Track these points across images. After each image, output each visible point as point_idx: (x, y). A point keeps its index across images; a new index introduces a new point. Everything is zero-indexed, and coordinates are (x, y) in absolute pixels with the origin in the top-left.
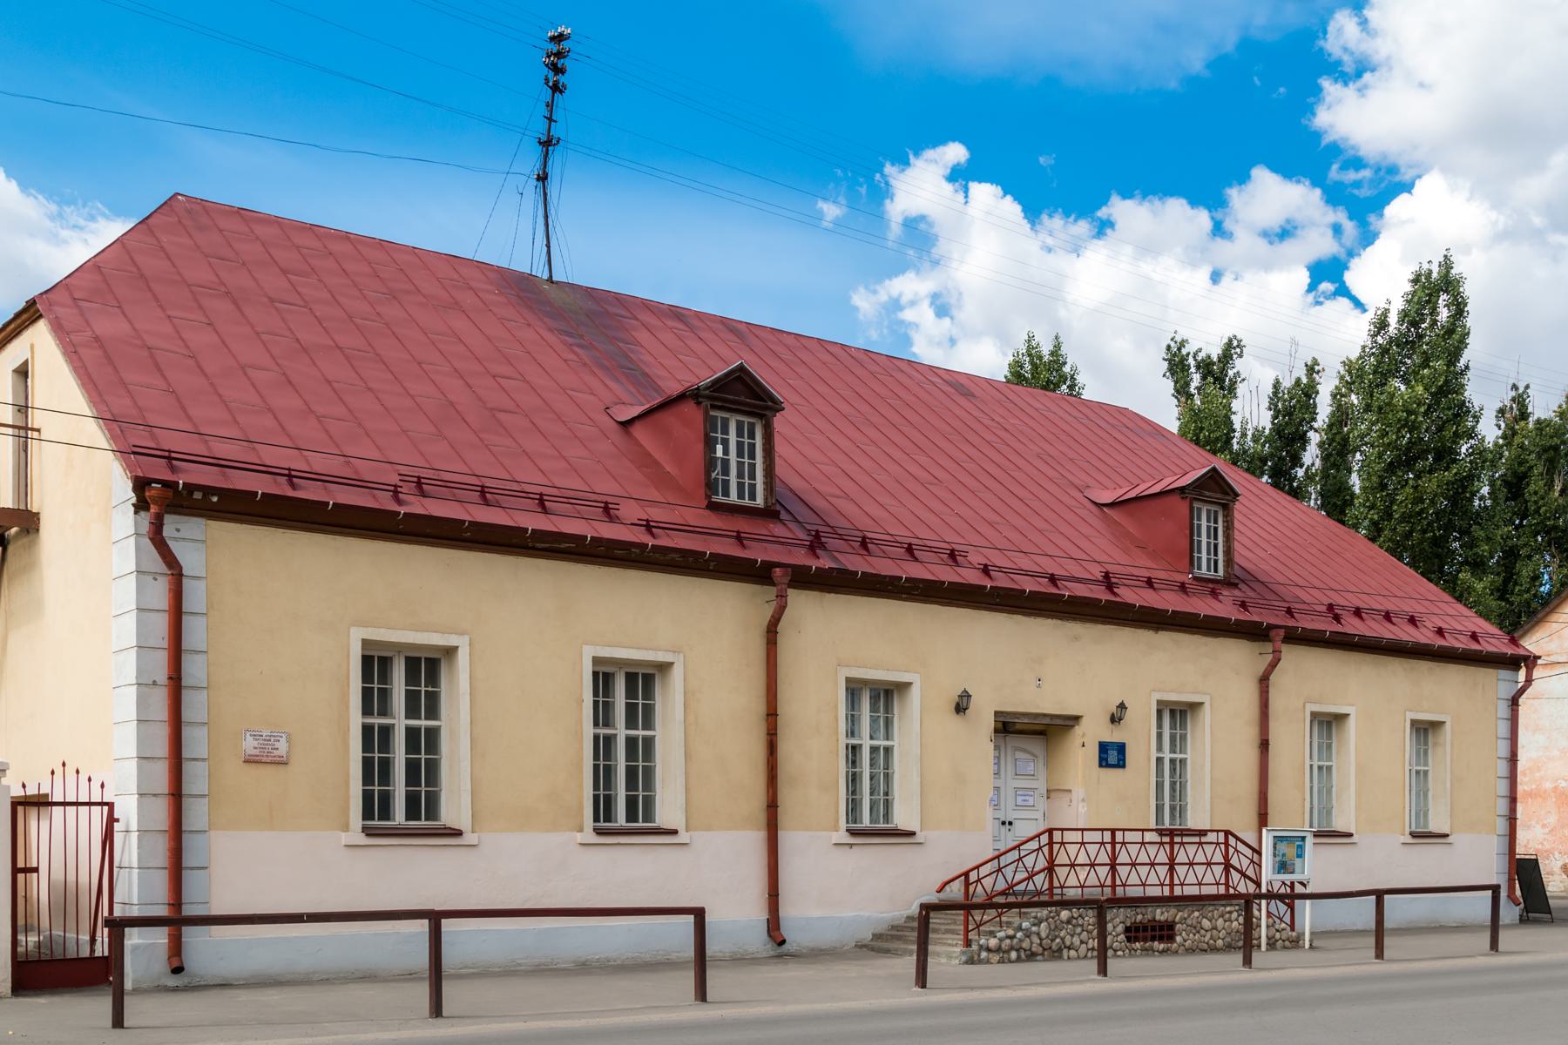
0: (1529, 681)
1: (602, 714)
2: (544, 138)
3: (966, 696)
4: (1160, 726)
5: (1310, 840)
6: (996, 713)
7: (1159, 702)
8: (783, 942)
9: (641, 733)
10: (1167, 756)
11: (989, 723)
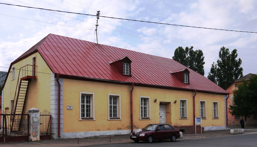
0: (228, 97)
1: (83, 101)
2: (96, 25)
3: (156, 100)
4: (181, 103)
5: (201, 119)
6: (160, 102)
7: (181, 100)
8: (60, 137)
9: (88, 104)
10: (113, 105)
11: (159, 103)
